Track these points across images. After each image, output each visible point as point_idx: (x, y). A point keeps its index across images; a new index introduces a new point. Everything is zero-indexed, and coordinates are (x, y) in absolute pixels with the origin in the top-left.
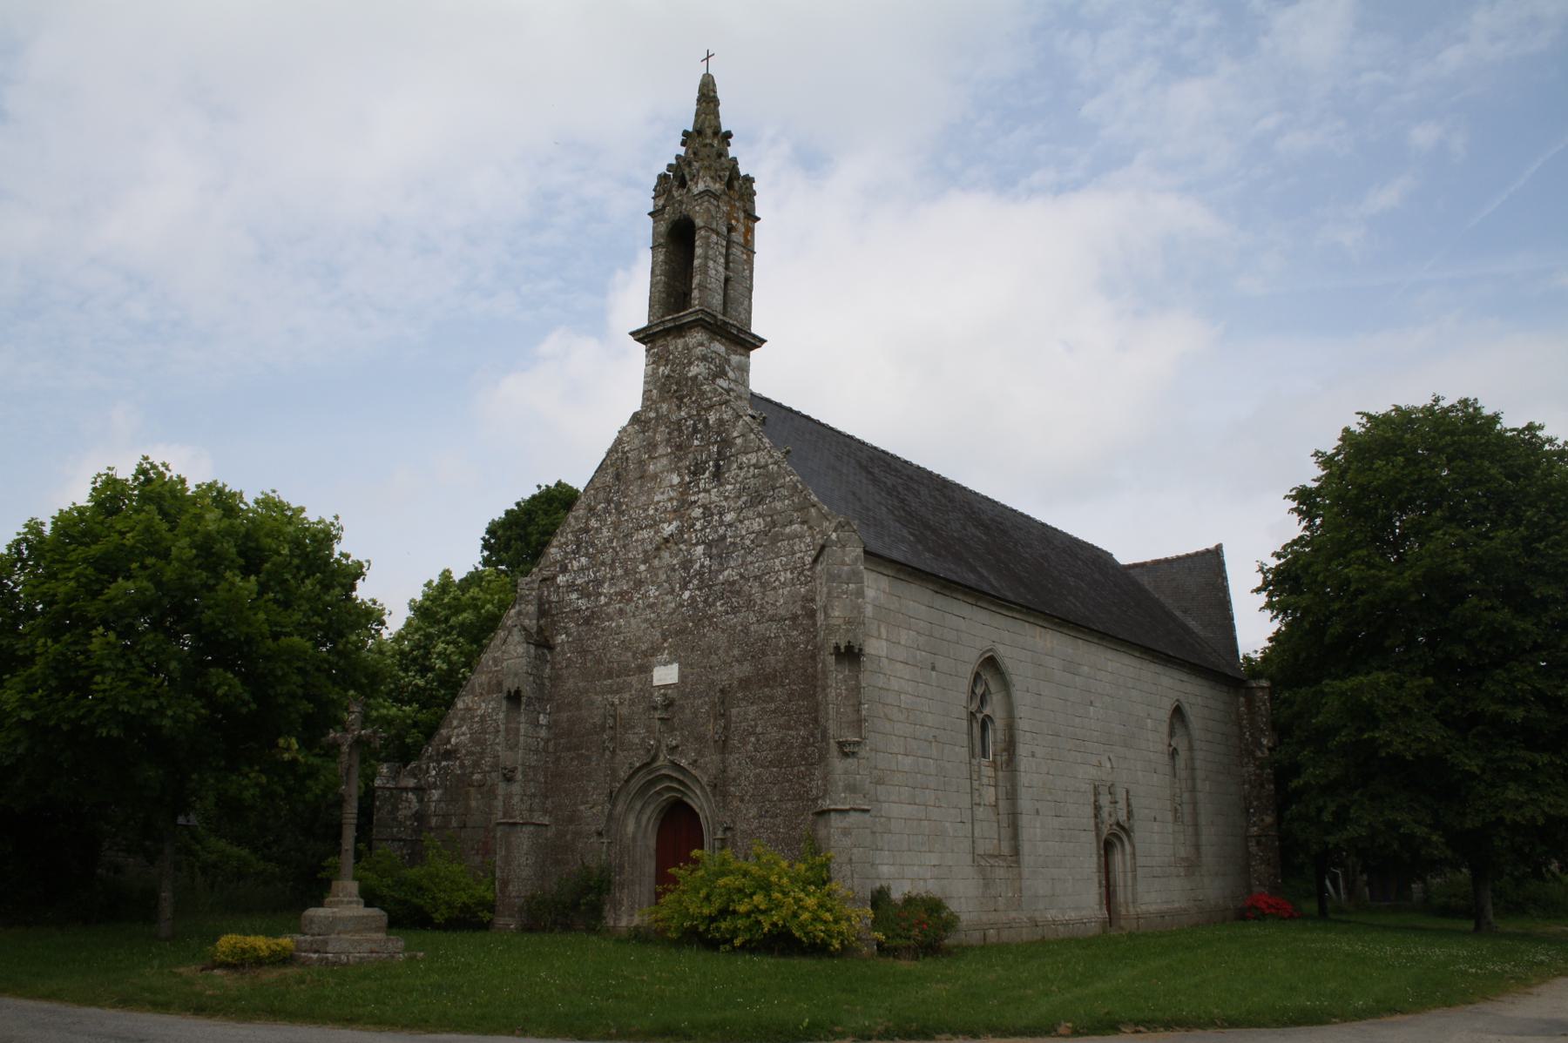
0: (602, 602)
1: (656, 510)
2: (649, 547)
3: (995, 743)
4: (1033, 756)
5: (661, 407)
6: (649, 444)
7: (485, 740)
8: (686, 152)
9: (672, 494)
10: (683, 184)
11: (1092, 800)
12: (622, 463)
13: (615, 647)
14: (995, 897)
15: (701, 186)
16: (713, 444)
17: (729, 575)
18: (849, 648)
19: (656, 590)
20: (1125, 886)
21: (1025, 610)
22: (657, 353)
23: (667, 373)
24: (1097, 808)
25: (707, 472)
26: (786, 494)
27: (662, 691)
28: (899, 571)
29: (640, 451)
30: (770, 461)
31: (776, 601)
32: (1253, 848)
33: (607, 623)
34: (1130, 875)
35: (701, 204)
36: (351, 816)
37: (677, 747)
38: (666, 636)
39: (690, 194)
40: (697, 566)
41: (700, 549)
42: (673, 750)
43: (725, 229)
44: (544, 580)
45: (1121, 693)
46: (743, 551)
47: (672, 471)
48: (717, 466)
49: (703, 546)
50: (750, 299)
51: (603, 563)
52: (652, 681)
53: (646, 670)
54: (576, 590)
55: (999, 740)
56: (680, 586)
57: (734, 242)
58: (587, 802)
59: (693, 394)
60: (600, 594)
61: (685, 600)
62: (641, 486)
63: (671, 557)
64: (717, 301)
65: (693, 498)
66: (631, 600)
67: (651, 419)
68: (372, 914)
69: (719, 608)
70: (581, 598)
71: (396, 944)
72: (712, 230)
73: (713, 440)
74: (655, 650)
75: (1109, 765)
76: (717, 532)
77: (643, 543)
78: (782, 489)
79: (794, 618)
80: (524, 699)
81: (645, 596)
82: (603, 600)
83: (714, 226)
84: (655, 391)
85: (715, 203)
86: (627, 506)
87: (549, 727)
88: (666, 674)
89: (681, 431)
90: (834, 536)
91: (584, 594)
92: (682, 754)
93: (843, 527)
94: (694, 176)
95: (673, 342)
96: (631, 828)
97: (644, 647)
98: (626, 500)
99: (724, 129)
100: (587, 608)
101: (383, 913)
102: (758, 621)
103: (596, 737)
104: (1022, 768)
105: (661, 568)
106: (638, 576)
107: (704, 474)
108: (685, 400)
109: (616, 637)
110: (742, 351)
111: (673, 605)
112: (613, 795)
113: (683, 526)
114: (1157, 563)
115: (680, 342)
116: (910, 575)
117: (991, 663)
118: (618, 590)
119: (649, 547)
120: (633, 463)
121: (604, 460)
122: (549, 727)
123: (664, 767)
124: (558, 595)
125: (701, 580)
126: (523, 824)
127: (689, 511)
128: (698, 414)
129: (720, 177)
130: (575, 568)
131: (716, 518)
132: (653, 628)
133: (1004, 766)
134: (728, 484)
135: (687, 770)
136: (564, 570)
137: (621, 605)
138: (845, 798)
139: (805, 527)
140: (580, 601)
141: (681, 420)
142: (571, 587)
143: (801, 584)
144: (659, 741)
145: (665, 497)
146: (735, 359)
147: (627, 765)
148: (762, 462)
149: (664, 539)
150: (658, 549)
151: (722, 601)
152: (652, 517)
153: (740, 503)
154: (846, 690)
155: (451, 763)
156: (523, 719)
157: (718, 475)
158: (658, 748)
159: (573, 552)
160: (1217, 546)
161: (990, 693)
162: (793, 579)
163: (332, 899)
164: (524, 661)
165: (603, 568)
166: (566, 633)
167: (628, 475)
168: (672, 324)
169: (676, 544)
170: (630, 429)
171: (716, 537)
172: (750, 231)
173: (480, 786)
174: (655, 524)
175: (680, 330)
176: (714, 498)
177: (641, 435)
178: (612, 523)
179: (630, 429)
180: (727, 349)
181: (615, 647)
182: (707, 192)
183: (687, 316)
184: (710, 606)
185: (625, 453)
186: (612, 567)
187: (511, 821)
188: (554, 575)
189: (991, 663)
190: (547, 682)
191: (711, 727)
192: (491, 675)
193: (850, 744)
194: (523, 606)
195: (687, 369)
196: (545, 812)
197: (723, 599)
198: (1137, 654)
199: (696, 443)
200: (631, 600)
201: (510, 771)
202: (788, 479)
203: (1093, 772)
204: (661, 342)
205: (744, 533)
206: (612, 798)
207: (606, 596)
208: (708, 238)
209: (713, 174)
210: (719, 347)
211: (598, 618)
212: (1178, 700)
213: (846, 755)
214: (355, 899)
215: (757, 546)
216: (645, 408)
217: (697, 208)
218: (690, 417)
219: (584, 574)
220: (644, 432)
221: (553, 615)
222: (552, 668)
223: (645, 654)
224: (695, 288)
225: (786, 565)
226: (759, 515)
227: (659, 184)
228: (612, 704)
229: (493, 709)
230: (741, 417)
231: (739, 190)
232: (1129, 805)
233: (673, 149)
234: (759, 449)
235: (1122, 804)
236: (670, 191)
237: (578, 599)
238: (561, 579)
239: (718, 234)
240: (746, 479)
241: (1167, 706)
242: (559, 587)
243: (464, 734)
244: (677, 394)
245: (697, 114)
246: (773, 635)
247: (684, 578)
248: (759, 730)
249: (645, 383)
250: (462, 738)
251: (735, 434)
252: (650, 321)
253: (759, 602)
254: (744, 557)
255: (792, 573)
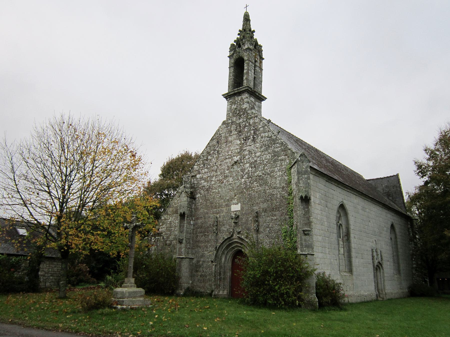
0: (213, 183)
1: (232, 152)
2: (229, 165)
3: (343, 233)
4: (355, 238)
5: (233, 119)
6: (229, 131)
7: (171, 230)
8: (240, 37)
9: (238, 147)
10: (239, 46)
11: (371, 254)
12: (219, 138)
13: (217, 198)
14: (346, 286)
15: (246, 47)
16: (252, 130)
17: (258, 173)
18: (306, 197)
19: (232, 179)
20: (381, 283)
21: (351, 189)
22: (231, 102)
23: (235, 107)
24: (373, 257)
25: (250, 140)
26: (279, 146)
27: (235, 213)
28: (316, 173)
29: (226, 134)
30: (273, 135)
31: (276, 182)
32: (414, 272)
33: (215, 190)
34: (382, 279)
35: (246, 52)
36: (133, 254)
37: (240, 232)
38: (236, 194)
39: (243, 49)
40: (247, 171)
41: (248, 165)
42: (239, 233)
43: (254, 61)
44: (192, 176)
45: (377, 219)
46: (263, 165)
47: (238, 139)
48: (254, 138)
49: (249, 164)
50: (262, 85)
51: (213, 171)
52: (231, 210)
53: (228, 206)
54: (203, 180)
55: (344, 232)
56: (241, 178)
57: (257, 66)
58: (208, 251)
59: (245, 114)
60: (212, 181)
61: (242, 182)
62: (226, 145)
63: (237, 168)
64: (252, 85)
65: (245, 148)
66: (223, 182)
67: (229, 123)
68: (140, 291)
69: (255, 185)
70: (205, 182)
71: (149, 301)
72: (250, 61)
73: (252, 129)
74: (232, 199)
75: (375, 242)
76: (254, 159)
77: (227, 164)
78: (277, 144)
79: (283, 188)
80: (186, 216)
81: (228, 181)
82: (213, 183)
83: (251, 60)
84: (231, 114)
85: (251, 52)
86: (221, 151)
87: (194, 225)
88: (236, 208)
89: (240, 126)
90: (299, 159)
91: (206, 180)
92: (242, 234)
93: (302, 156)
94: (244, 43)
95: (237, 97)
96: (223, 259)
97: (228, 198)
98: (221, 150)
99: (252, 30)
100: (207, 186)
101: (143, 290)
102: (269, 189)
103: (210, 229)
104: (352, 242)
105: (234, 171)
106: (225, 174)
107: (249, 140)
108: (242, 116)
109: (218, 195)
110: (259, 102)
111: (238, 184)
112: (217, 248)
113: (241, 158)
114: (377, 179)
115: (240, 98)
116: (319, 174)
117: (342, 207)
118: (218, 179)
119: (229, 165)
120: (223, 138)
121: (213, 137)
122: (194, 225)
123: (235, 239)
124: (197, 181)
125: (248, 175)
126: (186, 258)
127: (244, 153)
128: (246, 120)
129: (252, 44)
130: (203, 172)
131: (253, 154)
132: (231, 191)
133: (346, 241)
134: (257, 143)
135: (244, 240)
136: (199, 173)
137: (219, 184)
138: (305, 250)
139: (286, 157)
140: (205, 183)
141: (240, 123)
142: (202, 178)
143: (285, 176)
144: (234, 230)
145: (235, 148)
146: (257, 103)
147: (222, 238)
148: (270, 136)
149: (235, 162)
150: (233, 165)
151: (256, 182)
152: (230, 155)
153: (262, 149)
154: (304, 212)
155: (159, 237)
156: (186, 222)
157: (254, 140)
158: (233, 232)
159: (202, 167)
160: (397, 174)
161: (341, 216)
162: (282, 174)
163: (125, 285)
164: (186, 203)
165: (213, 172)
166: (200, 194)
167: (221, 141)
168: (237, 92)
169: (239, 164)
170: (222, 127)
171: (254, 161)
172: (261, 62)
173: (169, 245)
174: (232, 157)
175: (239, 94)
176: (252, 148)
177: (226, 128)
178: (216, 157)
179: (222, 127)
180: (255, 100)
181: (217, 198)
182: (248, 48)
183: (241, 89)
184: (252, 184)
185: (220, 134)
186: (216, 171)
187: (181, 257)
188: (196, 175)
189: (342, 207)
190: (193, 210)
191: (253, 225)
192: (173, 208)
193: (307, 231)
194: (186, 185)
195: (242, 106)
196: (193, 254)
197: (256, 181)
198: (381, 206)
199: (246, 130)
200: (223, 182)
201: (181, 240)
202: (279, 141)
203: (371, 244)
204: (233, 98)
205: (264, 159)
206: (217, 250)
207: (214, 181)
208: (249, 63)
209: (250, 43)
210: (253, 99)
211: (211, 189)
212: (392, 222)
213: (306, 235)
214: (133, 285)
215: (269, 164)
216: (228, 119)
217: (245, 54)
218: (244, 121)
219: (206, 174)
220: (227, 127)
221: (195, 188)
222: (195, 205)
223: (228, 200)
224: (245, 80)
225: (279, 169)
226: (269, 153)
227: (231, 47)
228: (217, 217)
229: (174, 219)
230: (262, 121)
231: (257, 48)
232: (381, 256)
233: (235, 36)
234: (269, 131)
235: (379, 256)
236: (235, 49)
237: (204, 182)
238: (198, 176)
239: (252, 62)
240: (264, 141)
241: (390, 224)
242: (197, 179)
243: (164, 228)
244: (239, 114)
245: (243, 25)
246: (275, 194)
247: (242, 175)
248: (270, 226)
249: (227, 111)
250: (163, 229)
251: (260, 127)
252: (228, 91)
253: (270, 182)
254: (264, 167)
255: (282, 172)
